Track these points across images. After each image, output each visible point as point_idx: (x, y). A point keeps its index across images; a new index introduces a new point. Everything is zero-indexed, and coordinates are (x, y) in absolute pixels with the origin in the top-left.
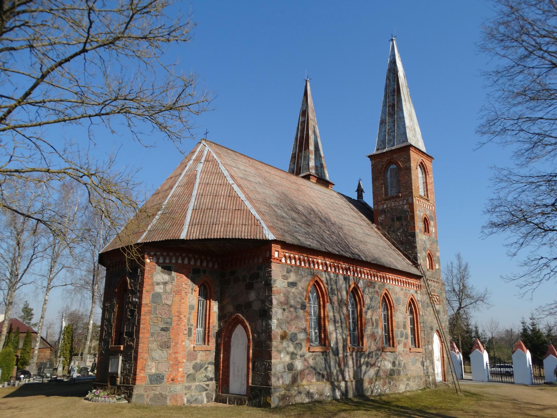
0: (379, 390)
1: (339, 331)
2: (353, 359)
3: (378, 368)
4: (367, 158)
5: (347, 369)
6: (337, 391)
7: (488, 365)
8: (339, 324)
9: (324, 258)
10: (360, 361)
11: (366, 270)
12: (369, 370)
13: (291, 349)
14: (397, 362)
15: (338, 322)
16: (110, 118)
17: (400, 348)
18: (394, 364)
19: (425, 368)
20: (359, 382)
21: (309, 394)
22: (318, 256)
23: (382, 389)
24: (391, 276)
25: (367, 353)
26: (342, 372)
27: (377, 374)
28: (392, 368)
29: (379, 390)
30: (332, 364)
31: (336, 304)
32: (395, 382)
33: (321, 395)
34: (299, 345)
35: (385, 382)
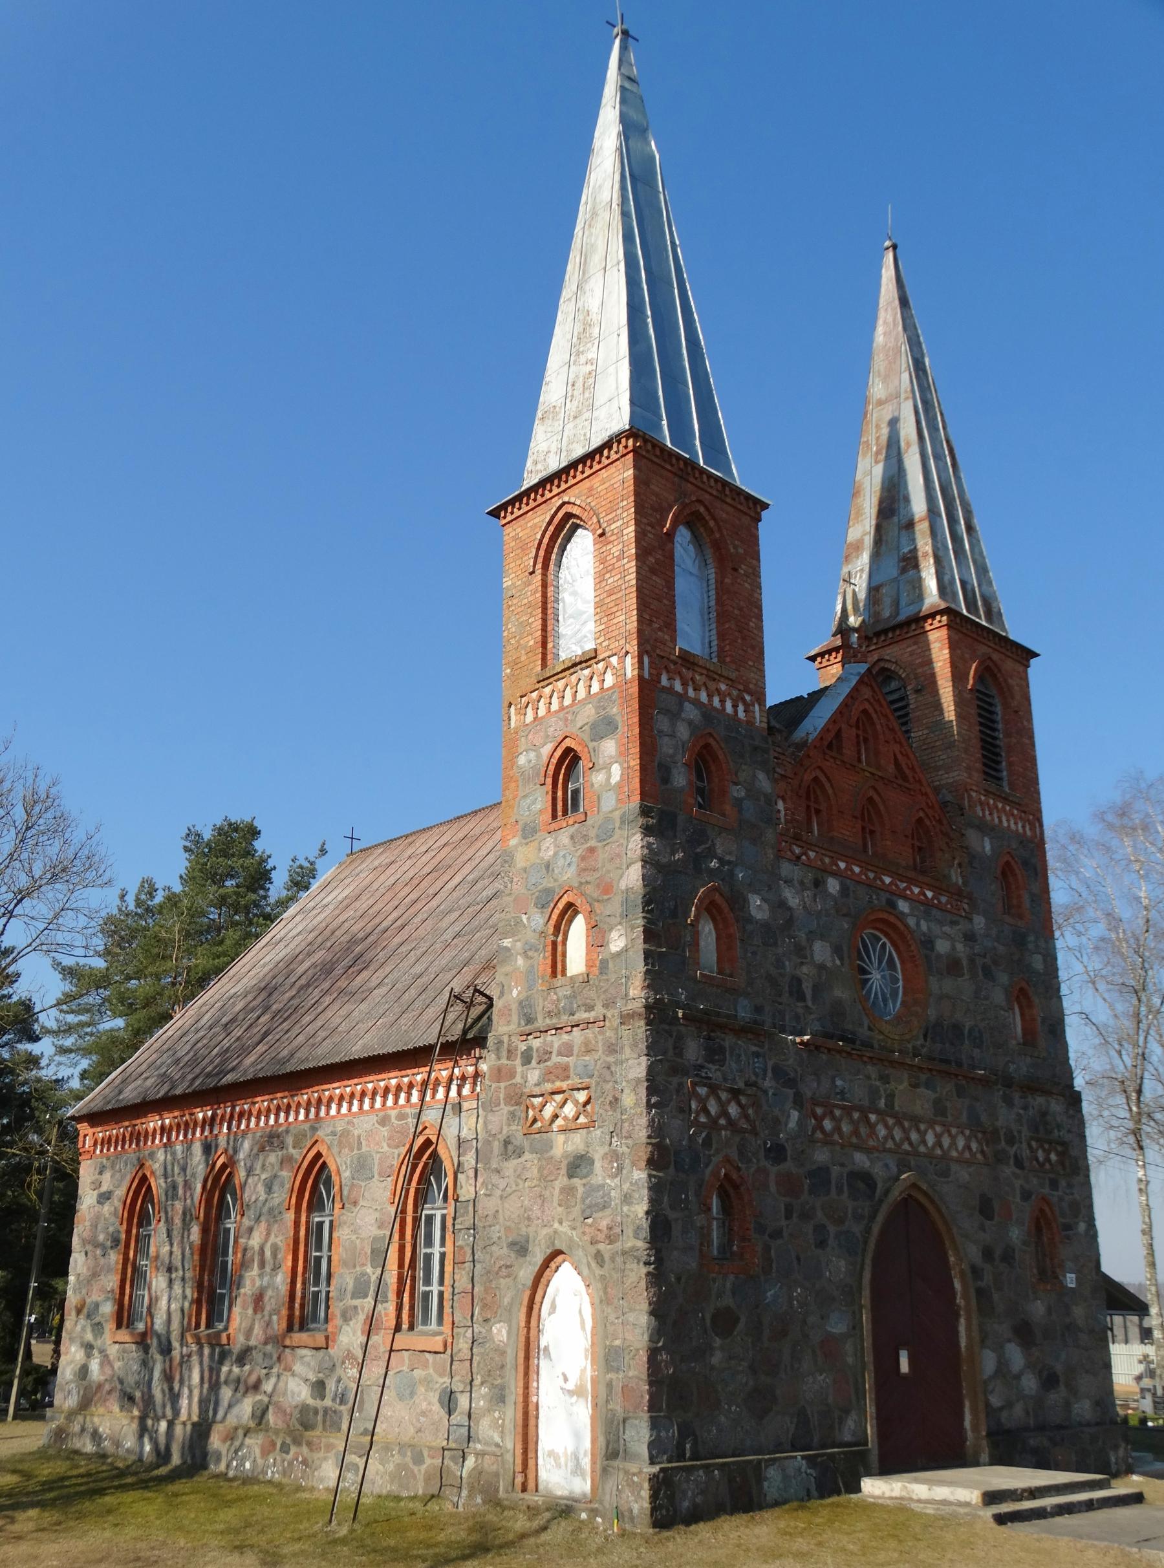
0: (248, 1465)
1: (177, 1289)
2: (201, 1363)
3: (266, 1399)
4: (1037, 651)
5: (186, 1391)
6: (146, 1440)
7: (837, 1426)
8: (181, 1273)
9: (161, 1115)
10: (219, 1371)
11: (262, 1102)
12: (238, 1401)
13: (89, 1336)
14: (331, 1386)
15: (176, 1270)
16: (1077, 1008)
17: (350, 1337)
18: (319, 1387)
19: (458, 1418)
20: (201, 1430)
21: (96, 1436)
22: (146, 1116)
23: (260, 1461)
24: (336, 1089)
25: (236, 1348)
26: (174, 1398)
27: (260, 1416)
28: (310, 1402)
29: (248, 1465)
30: (157, 1374)
31: (178, 1221)
32: (305, 1449)
33: (118, 1444)
34: (98, 1328)
35: (273, 1444)
